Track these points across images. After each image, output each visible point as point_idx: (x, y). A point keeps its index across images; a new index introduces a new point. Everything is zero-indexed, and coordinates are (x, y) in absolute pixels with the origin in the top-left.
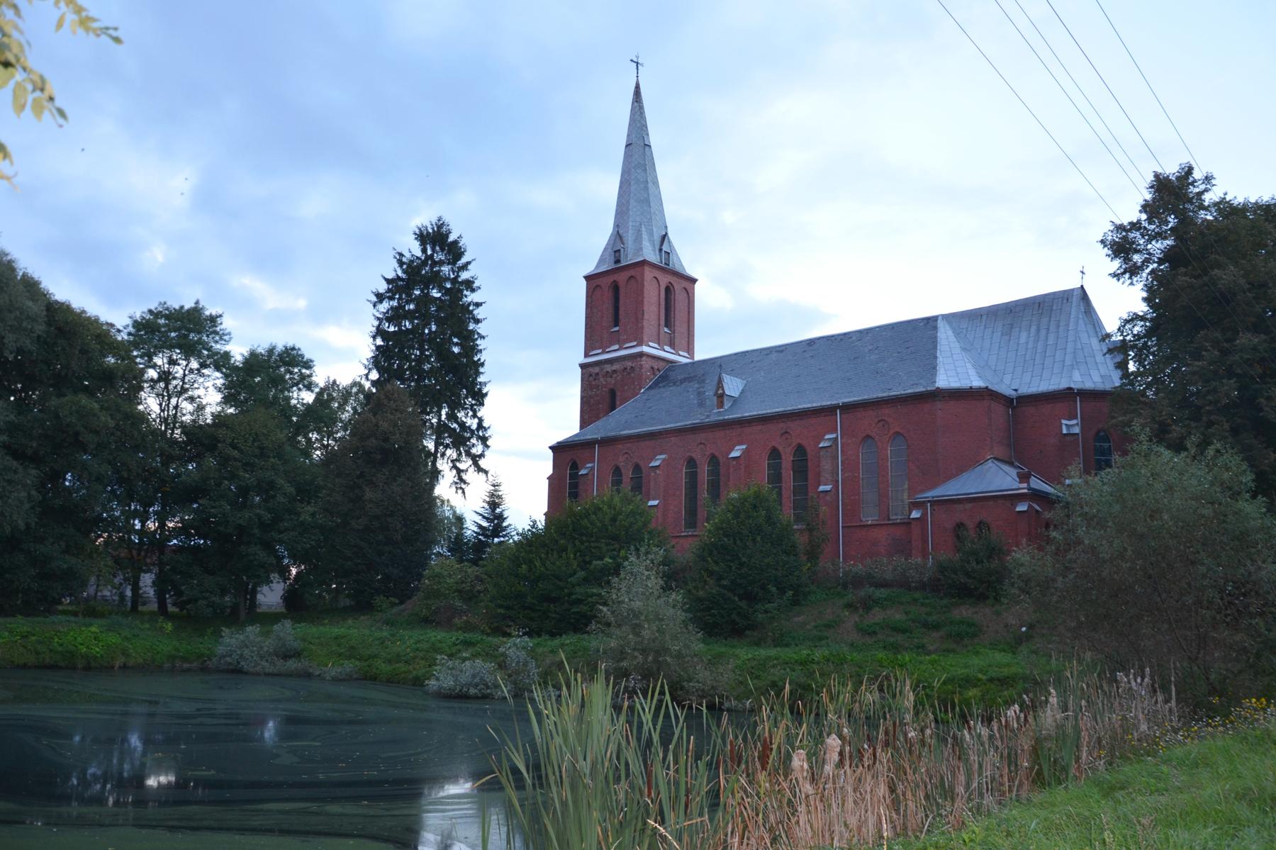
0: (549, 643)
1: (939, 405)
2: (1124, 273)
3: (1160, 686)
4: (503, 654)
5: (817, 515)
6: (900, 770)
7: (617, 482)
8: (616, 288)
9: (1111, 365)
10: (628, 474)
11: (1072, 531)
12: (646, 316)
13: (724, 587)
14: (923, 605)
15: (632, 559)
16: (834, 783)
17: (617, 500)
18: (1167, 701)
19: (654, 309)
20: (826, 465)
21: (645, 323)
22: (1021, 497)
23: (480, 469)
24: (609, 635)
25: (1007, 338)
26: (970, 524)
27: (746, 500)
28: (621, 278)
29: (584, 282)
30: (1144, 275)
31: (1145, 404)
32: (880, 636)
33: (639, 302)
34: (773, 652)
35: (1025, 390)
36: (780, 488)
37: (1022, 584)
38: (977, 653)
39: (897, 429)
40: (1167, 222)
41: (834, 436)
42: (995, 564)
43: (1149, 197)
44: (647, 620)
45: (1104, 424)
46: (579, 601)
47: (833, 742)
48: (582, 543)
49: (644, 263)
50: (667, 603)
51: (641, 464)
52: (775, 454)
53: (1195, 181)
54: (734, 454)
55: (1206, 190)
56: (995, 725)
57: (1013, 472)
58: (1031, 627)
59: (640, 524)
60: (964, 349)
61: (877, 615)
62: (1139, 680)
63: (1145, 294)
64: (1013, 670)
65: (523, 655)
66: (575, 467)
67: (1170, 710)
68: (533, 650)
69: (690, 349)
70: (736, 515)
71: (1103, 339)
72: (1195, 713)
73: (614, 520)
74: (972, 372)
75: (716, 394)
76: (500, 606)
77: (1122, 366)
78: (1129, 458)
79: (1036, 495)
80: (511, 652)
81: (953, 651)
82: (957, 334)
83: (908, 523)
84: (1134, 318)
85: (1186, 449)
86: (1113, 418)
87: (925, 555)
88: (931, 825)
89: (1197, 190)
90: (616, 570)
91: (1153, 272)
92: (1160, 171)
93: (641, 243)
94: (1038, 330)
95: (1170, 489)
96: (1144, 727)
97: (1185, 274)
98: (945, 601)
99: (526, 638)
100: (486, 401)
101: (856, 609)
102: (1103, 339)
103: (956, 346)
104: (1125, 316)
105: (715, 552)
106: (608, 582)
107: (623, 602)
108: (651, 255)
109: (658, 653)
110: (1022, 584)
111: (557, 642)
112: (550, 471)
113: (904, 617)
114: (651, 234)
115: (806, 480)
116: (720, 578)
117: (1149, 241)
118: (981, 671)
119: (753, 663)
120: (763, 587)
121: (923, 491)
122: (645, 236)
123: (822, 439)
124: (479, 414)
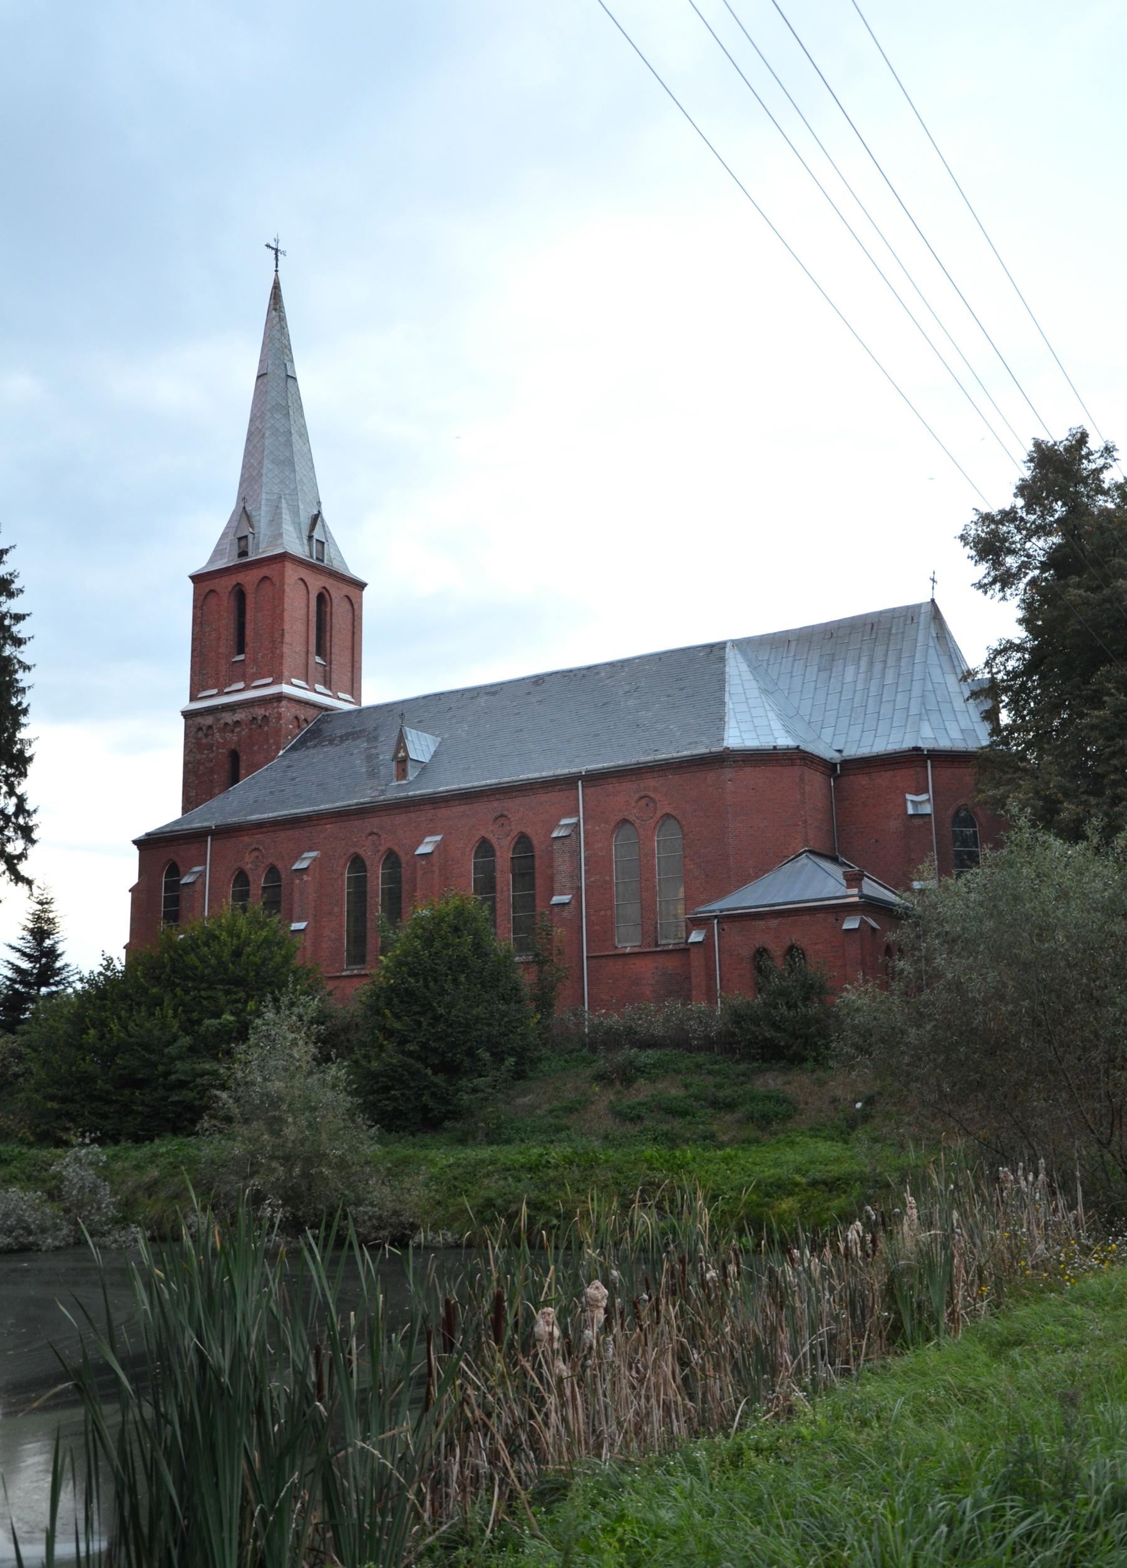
0: (133, 1153)
1: (729, 773)
2: (993, 583)
3: (1060, 1185)
4: (58, 1177)
5: (550, 941)
6: (693, 1333)
7: (242, 895)
8: (240, 595)
9: (976, 716)
10: (258, 881)
11: (929, 960)
13: (410, 1054)
14: (709, 1073)
15: (270, 1015)
16: (599, 1356)
17: (242, 922)
18: (1071, 1207)
19: (300, 627)
20: (562, 865)
21: (286, 649)
22: (849, 909)
23: (18, 878)
24: (231, 1137)
25: (824, 675)
26: (777, 950)
27: (442, 920)
28: (249, 579)
29: (190, 585)
30: (1022, 586)
31: (1024, 770)
32: (648, 1123)
33: (278, 616)
34: (486, 1152)
35: (853, 751)
36: (494, 898)
37: (857, 1039)
38: (792, 1144)
39: (668, 810)
40: (1052, 511)
41: (573, 820)
42: (814, 1009)
43: (1027, 474)
44: (291, 1109)
45: (968, 800)
46: (182, 1085)
47: (597, 1291)
48: (187, 992)
49: (284, 557)
50: (323, 1083)
51: (280, 865)
52: (485, 848)
53: (1090, 453)
54: (424, 849)
55: (1105, 467)
56: (828, 1253)
57: (837, 872)
58: (869, 1101)
59: (278, 959)
60: (765, 691)
61: (643, 1091)
62: (1031, 1178)
63: (1020, 614)
64: (846, 1168)
65: (90, 1174)
66: (174, 871)
67: (1076, 1222)
68: (106, 1166)
69: (354, 688)
70: (428, 942)
71: (964, 679)
72: (1112, 1224)
73: (237, 954)
74: (776, 725)
75: (395, 757)
76: (52, 1098)
77: (991, 716)
78: (1005, 852)
79: (870, 906)
80: (69, 1173)
81: (757, 1141)
82: (754, 668)
83: (686, 950)
84: (1008, 648)
85: (1086, 838)
86: (980, 791)
87: (711, 997)
88: (745, 1414)
89: (1093, 466)
90: (242, 1033)
91: (1033, 582)
92: (1043, 436)
93: (280, 525)
94: (871, 663)
95: (1063, 895)
96: (1040, 1247)
97: (1078, 586)
98: (743, 1067)
99: (96, 1148)
100: (31, 769)
101: (611, 1083)
102: (964, 679)
103: (753, 687)
104: (995, 645)
105: (396, 1001)
106: (229, 1053)
107: (253, 1084)
108: (295, 545)
109: (308, 1161)
110: (857, 1039)
111: (146, 1150)
112: (134, 879)
113: (682, 1093)
114: (296, 513)
115: (532, 886)
116: (403, 1041)
117: (1028, 538)
118: (798, 1170)
119: (458, 1172)
120: (470, 1053)
121: (709, 901)
122: (286, 516)
123: (555, 825)
124: (19, 790)
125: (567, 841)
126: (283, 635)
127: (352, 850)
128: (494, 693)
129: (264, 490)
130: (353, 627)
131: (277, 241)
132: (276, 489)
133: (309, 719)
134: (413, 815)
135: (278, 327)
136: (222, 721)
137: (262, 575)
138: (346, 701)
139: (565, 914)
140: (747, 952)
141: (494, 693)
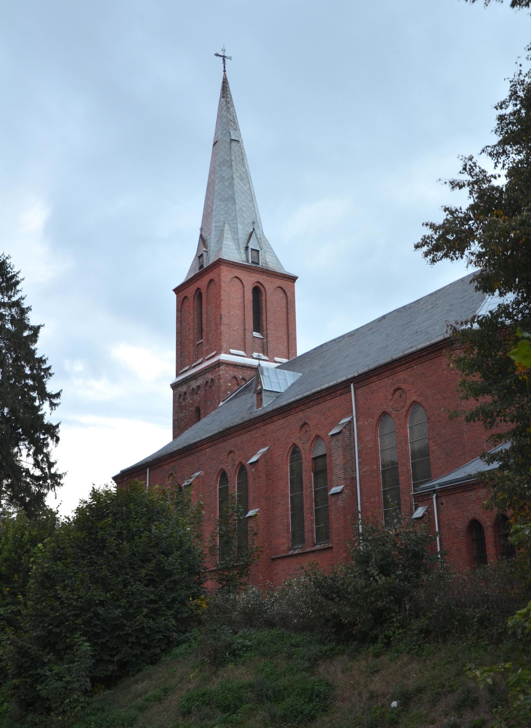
12: (225, 320)
19: (238, 312)
39: (414, 398)
41: (348, 419)
49: (220, 262)
114: (235, 232)
125: (340, 437)
126: (221, 318)
127: (220, 467)
129: (213, 220)
130: (287, 308)
131: (224, 50)
132: (222, 218)
133: (247, 378)
134: (253, 433)
135: (225, 109)
136: (191, 388)
137: (209, 279)
139: (340, 503)
140: (462, 525)
141: (352, 335)
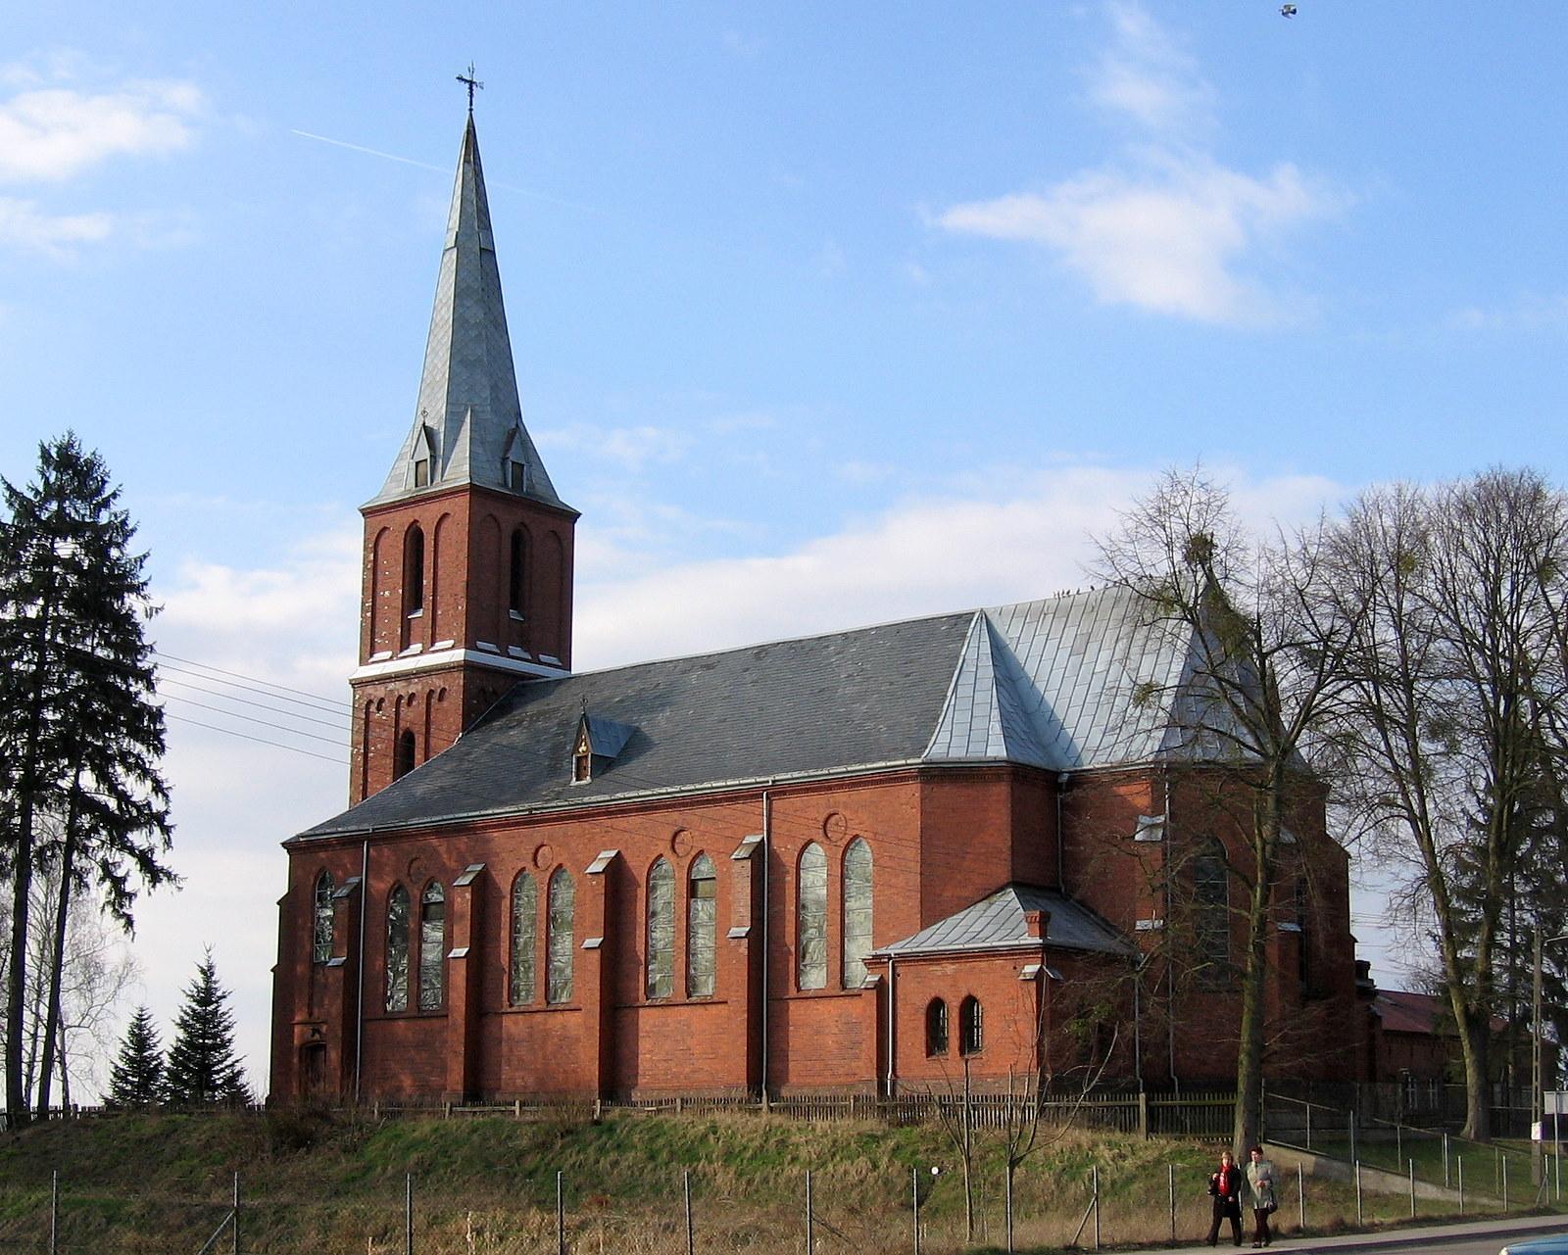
128: (708, 667)
131: (472, 71)
138: (550, 665)
141: (708, 667)
